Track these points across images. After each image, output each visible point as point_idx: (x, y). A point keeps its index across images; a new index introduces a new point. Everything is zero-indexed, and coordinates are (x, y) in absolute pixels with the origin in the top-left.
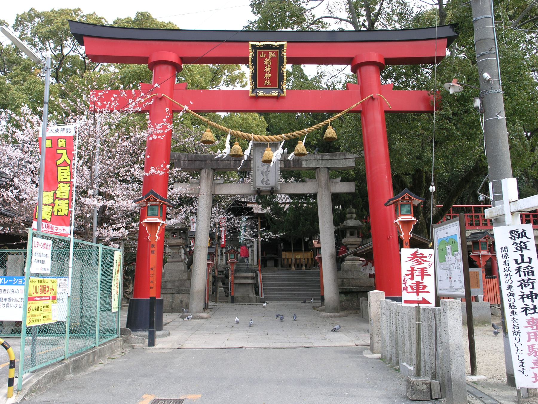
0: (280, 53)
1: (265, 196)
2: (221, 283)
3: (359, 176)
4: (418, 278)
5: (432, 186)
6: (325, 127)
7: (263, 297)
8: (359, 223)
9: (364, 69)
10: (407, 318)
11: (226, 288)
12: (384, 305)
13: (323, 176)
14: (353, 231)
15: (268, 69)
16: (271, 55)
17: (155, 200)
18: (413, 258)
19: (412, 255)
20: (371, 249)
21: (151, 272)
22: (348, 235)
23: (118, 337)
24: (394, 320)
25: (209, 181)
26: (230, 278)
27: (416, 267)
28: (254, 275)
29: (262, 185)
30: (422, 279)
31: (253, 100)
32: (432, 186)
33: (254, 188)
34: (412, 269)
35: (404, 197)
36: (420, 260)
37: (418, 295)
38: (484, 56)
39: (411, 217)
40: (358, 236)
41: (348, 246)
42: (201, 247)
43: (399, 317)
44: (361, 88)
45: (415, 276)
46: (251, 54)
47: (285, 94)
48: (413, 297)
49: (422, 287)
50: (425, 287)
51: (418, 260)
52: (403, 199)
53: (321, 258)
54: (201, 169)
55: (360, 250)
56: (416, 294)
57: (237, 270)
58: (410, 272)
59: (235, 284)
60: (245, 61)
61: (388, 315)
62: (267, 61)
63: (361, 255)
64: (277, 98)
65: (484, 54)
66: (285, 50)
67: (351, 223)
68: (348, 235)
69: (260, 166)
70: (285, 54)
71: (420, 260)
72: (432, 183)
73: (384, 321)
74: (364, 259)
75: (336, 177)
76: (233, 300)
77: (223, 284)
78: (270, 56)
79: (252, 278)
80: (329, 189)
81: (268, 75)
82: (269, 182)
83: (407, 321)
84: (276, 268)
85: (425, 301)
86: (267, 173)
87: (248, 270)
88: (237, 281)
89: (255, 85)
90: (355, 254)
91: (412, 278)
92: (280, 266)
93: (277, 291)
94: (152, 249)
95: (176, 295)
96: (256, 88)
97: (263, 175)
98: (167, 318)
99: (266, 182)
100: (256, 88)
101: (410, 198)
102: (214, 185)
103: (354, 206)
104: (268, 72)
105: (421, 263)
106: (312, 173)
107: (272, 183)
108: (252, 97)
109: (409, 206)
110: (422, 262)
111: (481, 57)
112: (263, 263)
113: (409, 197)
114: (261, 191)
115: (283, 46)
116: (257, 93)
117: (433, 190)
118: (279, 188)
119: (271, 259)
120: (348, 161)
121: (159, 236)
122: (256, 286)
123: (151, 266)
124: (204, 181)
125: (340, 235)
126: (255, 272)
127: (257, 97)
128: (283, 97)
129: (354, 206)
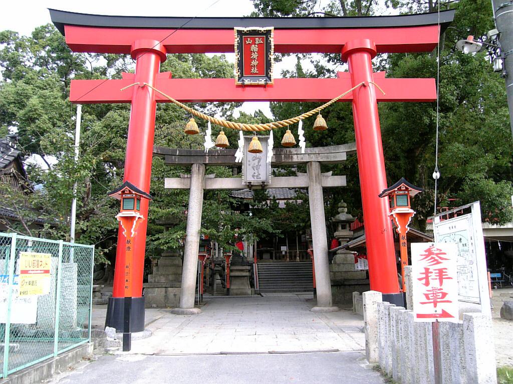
0: (267, 39)
1: (260, 191)
2: (218, 275)
3: (351, 169)
4: (434, 283)
5: (436, 172)
6: (314, 117)
7: (258, 289)
8: (350, 216)
9: (355, 57)
10: (413, 328)
11: (223, 279)
12: (382, 308)
13: (315, 169)
14: (345, 224)
15: (255, 56)
16: (258, 41)
17: (130, 193)
18: (427, 256)
19: (426, 251)
20: (364, 243)
21: (127, 270)
22: (340, 228)
23: (88, 342)
24: (395, 328)
25: (200, 176)
26: (226, 271)
27: (431, 269)
28: (248, 268)
29: (253, 179)
30: (441, 283)
31: (240, 89)
32: (436, 172)
33: (245, 182)
34: (427, 271)
35: (401, 187)
36: (437, 258)
37: (435, 306)
38: (504, 9)
39: (408, 209)
40: (350, 230)
41: (340, 240)
42: (192, 241)
43: (401, 326)
44: (352, 75)
45: (431, 281)
46: (236, 40)
47: (272, 82)
48: (429, 309)
49: (440, 294)
50: (444, 295)
51: (434, 258)
52: (400, 189)
53: (313, 251)
54: (192, 164)
55: (352, 243)
56: (433, 304)
57: (233, 264)
58: (424, 276)
59: (230, 276)
60: (229, 48)
61: (387, 321)
62: (254, 48)
63: (353, 249)
64: (264, 86)
65: (505, 6)
66: (272, 36)
67: (343, 216)
68: (340, 228)
69: (251, 161)
70: (272, 40)
71: (437, 258)
72: (436, 168)
73: (382, 327)
74: (356, 252)
75: (328, 171)
76: (228, 293)
77: (221, 276)
78: (257, 42)
79: (249, 271)
80: (320, 183)
81: (255, 63)
82: (260, 176)
83: (413, 332)
84: (271, 260)
85: (445, 314)
86: (257, 167)
87: (243, 264)
88: (233, 274)
89: (242, 73)
90: (347, 248)
91: (427, 284)
92: (274, 258)
93: (271, 283)
94: (128, 245)
95: (169, 289)
96: (242, 76)
97: (254, 169)
98: (149, 314)
99: (257, 176)
100: (242, 76)
101: (407, 189)
102: (205, 180)
103: (348, 200)
104: (254, 59)
105: (438, 263)
106: (303, 167)
107: (263, 178)
108: (238, 86)
109: (406, 197)
110: (440, 260)
111: (501, 10)
112: (259, 255)
113: (406, 187)
114: (252, 186)
115: (270, 31)
116: (243, 81)
117: (437, 177)
118: (270, 182)
119: (267, 252)
120: (339, 154)
121: (135, 231)
122: (251, 278)
123: (127, 264)
124: (195, 175)
125: (331, 227)
126: (251, 265)
127: (243, 86)
128: (271, 86)
129: (348, 200)
